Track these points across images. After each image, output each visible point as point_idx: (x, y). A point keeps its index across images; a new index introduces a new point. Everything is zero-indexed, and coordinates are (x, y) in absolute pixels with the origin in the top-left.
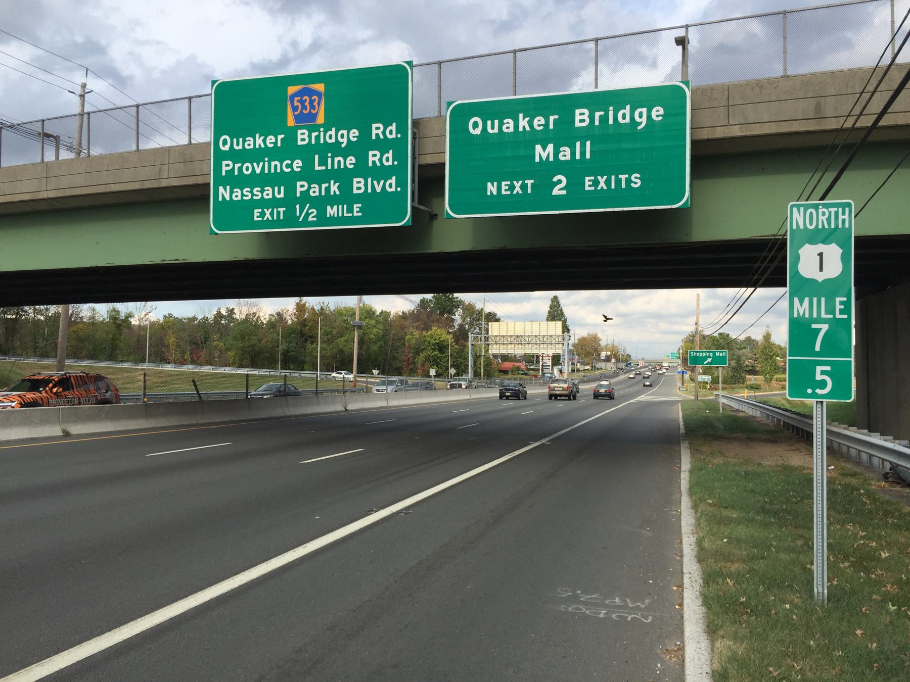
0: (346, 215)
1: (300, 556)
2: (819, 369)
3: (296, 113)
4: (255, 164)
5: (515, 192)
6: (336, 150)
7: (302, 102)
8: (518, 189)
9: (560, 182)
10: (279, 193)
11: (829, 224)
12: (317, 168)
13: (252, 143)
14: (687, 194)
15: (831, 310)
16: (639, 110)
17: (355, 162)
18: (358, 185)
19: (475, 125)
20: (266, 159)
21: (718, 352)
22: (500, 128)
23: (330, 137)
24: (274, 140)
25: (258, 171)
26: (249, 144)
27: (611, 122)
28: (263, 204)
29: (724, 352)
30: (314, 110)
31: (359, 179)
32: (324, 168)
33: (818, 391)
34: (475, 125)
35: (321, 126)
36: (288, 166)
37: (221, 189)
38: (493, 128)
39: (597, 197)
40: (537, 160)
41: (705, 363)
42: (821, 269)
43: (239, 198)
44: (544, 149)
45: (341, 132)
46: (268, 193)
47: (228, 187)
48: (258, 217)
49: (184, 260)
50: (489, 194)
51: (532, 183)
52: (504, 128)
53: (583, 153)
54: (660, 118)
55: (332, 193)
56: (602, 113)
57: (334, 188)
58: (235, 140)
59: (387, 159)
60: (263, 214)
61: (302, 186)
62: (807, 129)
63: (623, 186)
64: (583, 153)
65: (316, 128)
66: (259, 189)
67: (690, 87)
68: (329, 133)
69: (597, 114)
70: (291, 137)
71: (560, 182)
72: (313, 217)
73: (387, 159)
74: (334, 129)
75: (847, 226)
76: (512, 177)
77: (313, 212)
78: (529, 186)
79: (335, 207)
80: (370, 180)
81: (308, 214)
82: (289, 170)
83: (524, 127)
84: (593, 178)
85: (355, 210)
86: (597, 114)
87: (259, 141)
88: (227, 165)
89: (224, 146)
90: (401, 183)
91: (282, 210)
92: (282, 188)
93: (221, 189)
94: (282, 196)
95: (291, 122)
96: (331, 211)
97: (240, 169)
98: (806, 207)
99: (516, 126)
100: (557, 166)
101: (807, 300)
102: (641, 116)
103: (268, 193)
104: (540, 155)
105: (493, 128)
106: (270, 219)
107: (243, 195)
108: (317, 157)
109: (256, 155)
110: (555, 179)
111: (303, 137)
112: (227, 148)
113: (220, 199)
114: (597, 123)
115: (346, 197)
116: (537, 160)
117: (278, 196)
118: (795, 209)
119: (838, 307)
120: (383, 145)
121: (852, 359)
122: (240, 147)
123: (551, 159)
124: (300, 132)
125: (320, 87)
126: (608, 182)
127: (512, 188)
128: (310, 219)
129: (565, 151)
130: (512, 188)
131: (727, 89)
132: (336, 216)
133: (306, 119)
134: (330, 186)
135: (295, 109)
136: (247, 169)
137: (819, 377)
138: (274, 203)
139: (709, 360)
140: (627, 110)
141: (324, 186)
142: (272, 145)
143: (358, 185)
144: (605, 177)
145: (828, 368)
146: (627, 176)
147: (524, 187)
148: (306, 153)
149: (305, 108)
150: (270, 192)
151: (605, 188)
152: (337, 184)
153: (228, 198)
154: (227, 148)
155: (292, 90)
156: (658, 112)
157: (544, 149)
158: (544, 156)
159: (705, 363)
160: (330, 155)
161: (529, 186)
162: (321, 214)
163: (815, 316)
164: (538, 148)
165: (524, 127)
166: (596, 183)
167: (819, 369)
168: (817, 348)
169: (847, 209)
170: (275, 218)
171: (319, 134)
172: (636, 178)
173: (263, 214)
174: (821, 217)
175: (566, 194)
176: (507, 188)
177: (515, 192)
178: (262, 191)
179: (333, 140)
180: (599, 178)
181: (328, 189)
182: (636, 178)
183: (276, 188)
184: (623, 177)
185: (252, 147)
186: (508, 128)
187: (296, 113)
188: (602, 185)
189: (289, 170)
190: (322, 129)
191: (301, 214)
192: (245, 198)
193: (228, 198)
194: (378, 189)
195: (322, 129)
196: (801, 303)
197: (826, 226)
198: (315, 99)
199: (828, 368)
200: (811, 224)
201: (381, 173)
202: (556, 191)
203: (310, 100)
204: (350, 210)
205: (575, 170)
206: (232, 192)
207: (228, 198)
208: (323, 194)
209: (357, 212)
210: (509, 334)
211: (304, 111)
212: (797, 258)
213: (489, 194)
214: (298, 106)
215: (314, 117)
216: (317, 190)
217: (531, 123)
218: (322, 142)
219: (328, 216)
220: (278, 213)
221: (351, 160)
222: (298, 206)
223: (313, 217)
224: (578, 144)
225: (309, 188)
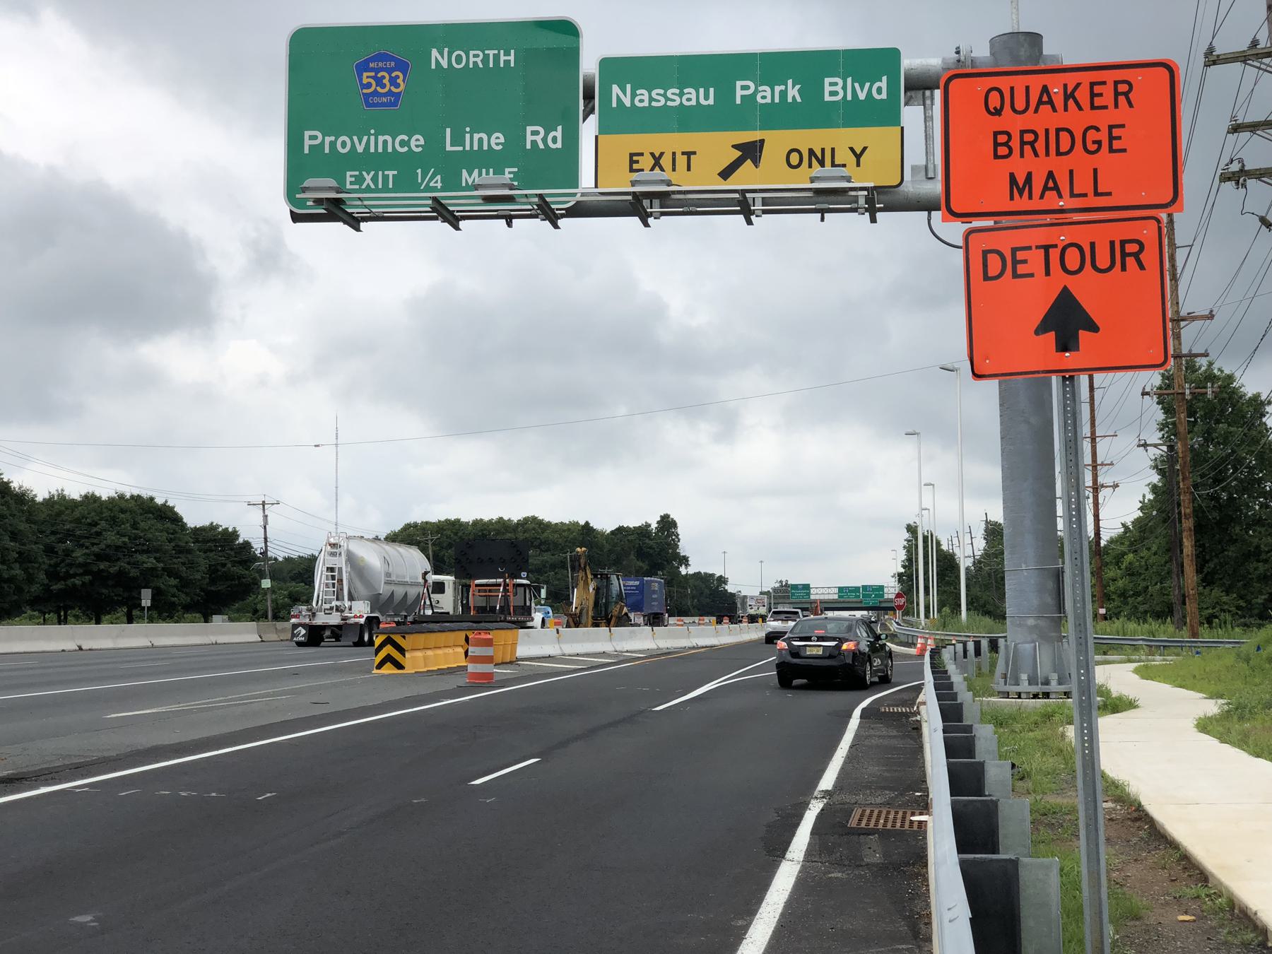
1: (776, 877)
4: (355, 138)
10: (707, 98)
12: (449, 148)
17: (503, 141)
20: (372, 131)
25: (360, 149)
31: (763, 101)
36: (403, 143)
37: (615, 89)
47: (628, 86)
55: (790, 100)
59: (555, 140)
61: (744, 88)
66: (677, 91)
73: (555, 140)
82: (406, 149)
92: (712, 90)
94: (711, 101)
97: (333, 144)
107: (651, 99)
108: (448, 130)
117: (703, 102)
134: (786, 88)
136: (344, 144)
141: (778, 89)
150: (693, 96)
152: (798, 87)
165: (794, 97)
178: (681, 95)
181: (783, 94)
183: (702, 90)
189: (406, 149)
192: (654, 104)
193: (627, 102)
194: (862, 96)
206: (634, 95)
207: (627, 102)
208: (777, 100)
216: (768, 94)
225: (756, 91)
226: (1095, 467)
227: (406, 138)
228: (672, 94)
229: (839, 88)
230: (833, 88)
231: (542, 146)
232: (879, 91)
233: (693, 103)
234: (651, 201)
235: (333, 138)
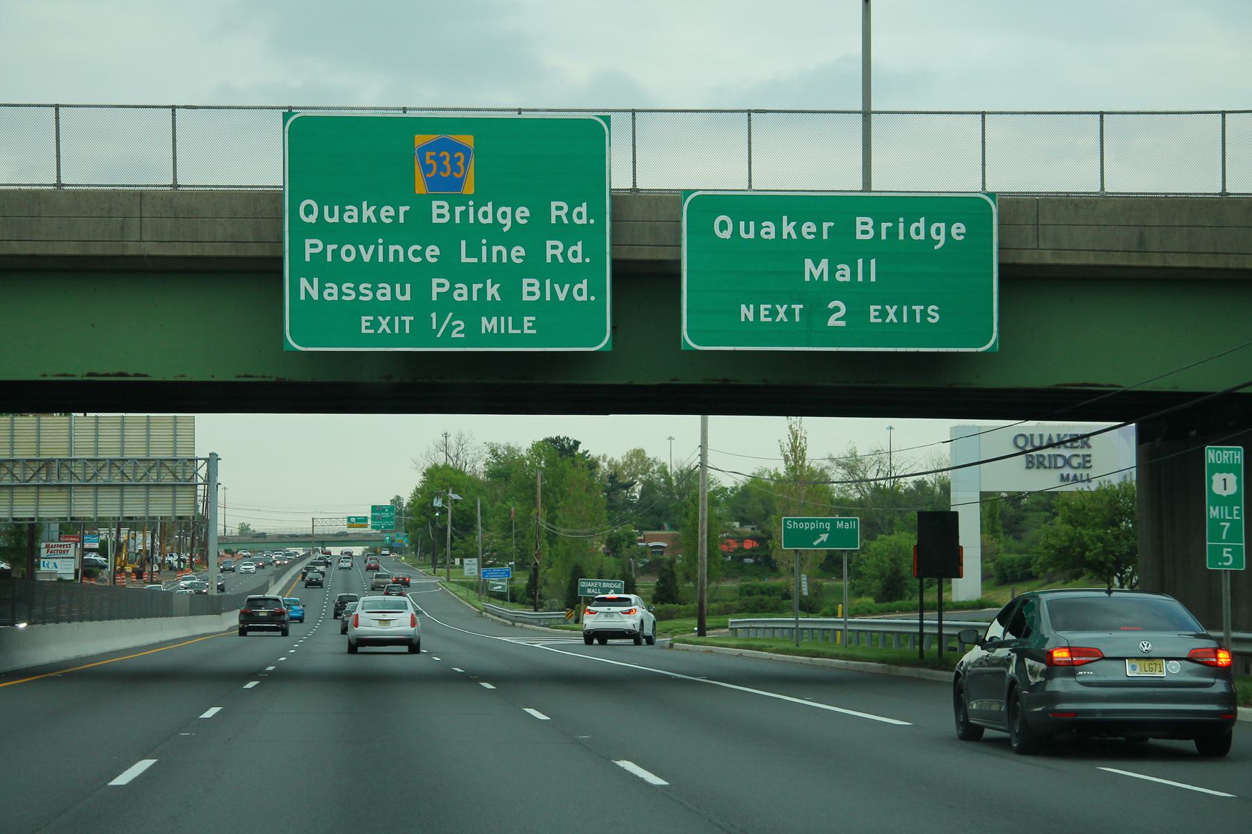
0: (511, 331)
2: (1225, 550)
3: (428, 175)
4: (361, 247)
5: (778, 320)
6: (494, 233)
7: (439, 161)
8: (782, 315)
9: (837, 309)
10: (403, 293)
11: (1229, 461)
12: (464, 259)
13: (355, 213)
14: (995, 335)
15: (1231, 514)
16: (936, 225)
18: (530, 289)
19: (723, 226)
20: (380, 241)
21: (840, 520)
22: (757, 233)
23: (485, 215)
24: (392, 213)
25: (367, 258)
26: (351, 215)
27: (901, 237)
28: (376, 308)
29: (853, 520)
30: (459, 173)
31: (350, 221)
32: (475, 260)
33: (1225, 564)
34: (723, 226)
35: (469, 197)
36: (415, 253)
37: (304, 282)
38: (747, 232)
39: (885, 332)
40: (807, 278)
41: (815, 543)
42: (1225, 489)
43: (335, 298)
44: (816, 265)
45: (502, 209)
46: (385, 292)
47: (316, 280)
48: (367, 328)
49: (137, 375)
50: (743, 319)
51: (800, 309)
52: (763, 232)
53: (867, 273)
54: (962, 237)
56: (890, 225)
57: (492, 291)
58: (326, 208)
60: (375, 324)
61: (440, 285)
62: (1129, 264)
63: (918, 320)
64: (867, 273)
65: (463, 200)
67: (997, 201)
68: (483, 209)
69: (884, 226)
70: (420, 214)
71: (837, 309)
72: (458, 332)
73: (575, 254)
74: (490, 204)
75: (1239, 462)
76: (774, 298)
77: (460, 325)
78: (797, 312)
79: (494, 319)
80: (548, 282)
81: (450, 328)
82: (419, 260)
83: (789, 234)
84: (879, 307)
85: (526, 325)
86: (884, 226)
87: (368, 213)
88: (314, 246)
89: (307, 216)
90: (595, 289)
91: (408, 319)
92: (408, 286)
93: (304, 282)
94: (407, 297)
95: (421, 187)
96: (488, 325)
98: (1216, 450)
99: (779, 232)
100: (834, 289)
101: (1217, 507)
102: (938, 233)
103: (385, 292)
104: (811, 272)
105: (747, 232)
106: (388, 331)
107: (341, 293)
108: (463, 243)
109: (364, 233)
110: (831, 305)
111: (440, 211)
112: (312, 219)
113: (303, 297)
114: (884, 237)
115: (511, 305)
116: (807, 278)
118: (1209, 450)
119: (1235, 512)
120: (567, 233)
121: (1244, 544)
122: (336, 219)
123: (826, 278)
124: (435, 203)
125: (468, 140)
126: (899, 314)
127: (773, 313)
128: (454, 335)
129: (844, 270)
130: (773, 313)
131: (1036, 204)
132: (495, 331)
133: (447, 186)
135: (426, 169)
136: (348, 253)
137: (1225, 555)
138: (393, 308)
139: (824, 537)
140: (921, 224)
141: (476, 287)
142: (389, 221)
143: (530, 289)
144: (895, 307)
145: (1230, 550)
146: (922, 307)
147: (790, 313)
148: (448, 235)
149: (445, 170)
150: (388, 291)
151: (895, 320)
152: (497, 286)
153: (315, 297)
154: (312, 219)
155: (421, 140)
156: (958, 229)
157: (816, 265)
158: (816, 274)
159: (815, 543)
160: (484, 241)
161: (797, 312)
162: (472, 330)
163: (1222, 517)
164: (809, 263)
165: (789, 234)
166: (883, 314)
167: (1225, 550)
168: (1224, 538)
169: (1239, 452)
170: (397, 331)
171: (467, 210)
172: (933, 310)
173: (375, 324)
174: (1224, 456)
175: (845, 325)
176: (767, 312)
177: (778, 320)
178: (374, 290)
179: (490, 220)
180: (888, 307)
181: (482, 292)
182: (933, 310)
184: (918, 308)
185: (355, 220)
186: (767, 233)
187: (428, 175)
188: (891, 317)
189: (419, 260)
190: (471, 203)
191: (439, 327)
192: (344, 298)
193: (315, 297)
194: (562, 297)
195: (471, 203)
196: (1214, 509)
197: (1228, 462)
198: (459, 157)
199: (1230, 550)
200: (1219, 454)
201: (564, 273)
202: (832, 322)
203: (452, 158)
204: (518, 324)
205: (857, 296)
206: (321, 289)
207: (315, 295)
208: (475, 298)
209: (529, 328)
210: (20, 454)
211: (442, 174)
212: (1211, 482)
213: (743, 319)
214: (431, 165)
215: (457, 184)
216: (465, 291)
217: (798, 229)
218: (471, 221)
219: (483, 331)
220: (402, 323)
221: (518, 253)
222: (434, 315)
223: (458, 332)
224: (860, 261)
225: (452, 289)
226: (765, 628)
227: (419, 248)
228: (347, 288)
229: (536, 289)
230: (531, 289)
231: (561, 260)
232: (580, 292)
233: (388, 298)
234: (1102, 188)
235: (335, 247)
